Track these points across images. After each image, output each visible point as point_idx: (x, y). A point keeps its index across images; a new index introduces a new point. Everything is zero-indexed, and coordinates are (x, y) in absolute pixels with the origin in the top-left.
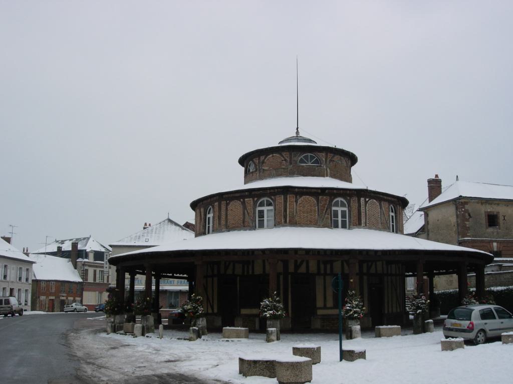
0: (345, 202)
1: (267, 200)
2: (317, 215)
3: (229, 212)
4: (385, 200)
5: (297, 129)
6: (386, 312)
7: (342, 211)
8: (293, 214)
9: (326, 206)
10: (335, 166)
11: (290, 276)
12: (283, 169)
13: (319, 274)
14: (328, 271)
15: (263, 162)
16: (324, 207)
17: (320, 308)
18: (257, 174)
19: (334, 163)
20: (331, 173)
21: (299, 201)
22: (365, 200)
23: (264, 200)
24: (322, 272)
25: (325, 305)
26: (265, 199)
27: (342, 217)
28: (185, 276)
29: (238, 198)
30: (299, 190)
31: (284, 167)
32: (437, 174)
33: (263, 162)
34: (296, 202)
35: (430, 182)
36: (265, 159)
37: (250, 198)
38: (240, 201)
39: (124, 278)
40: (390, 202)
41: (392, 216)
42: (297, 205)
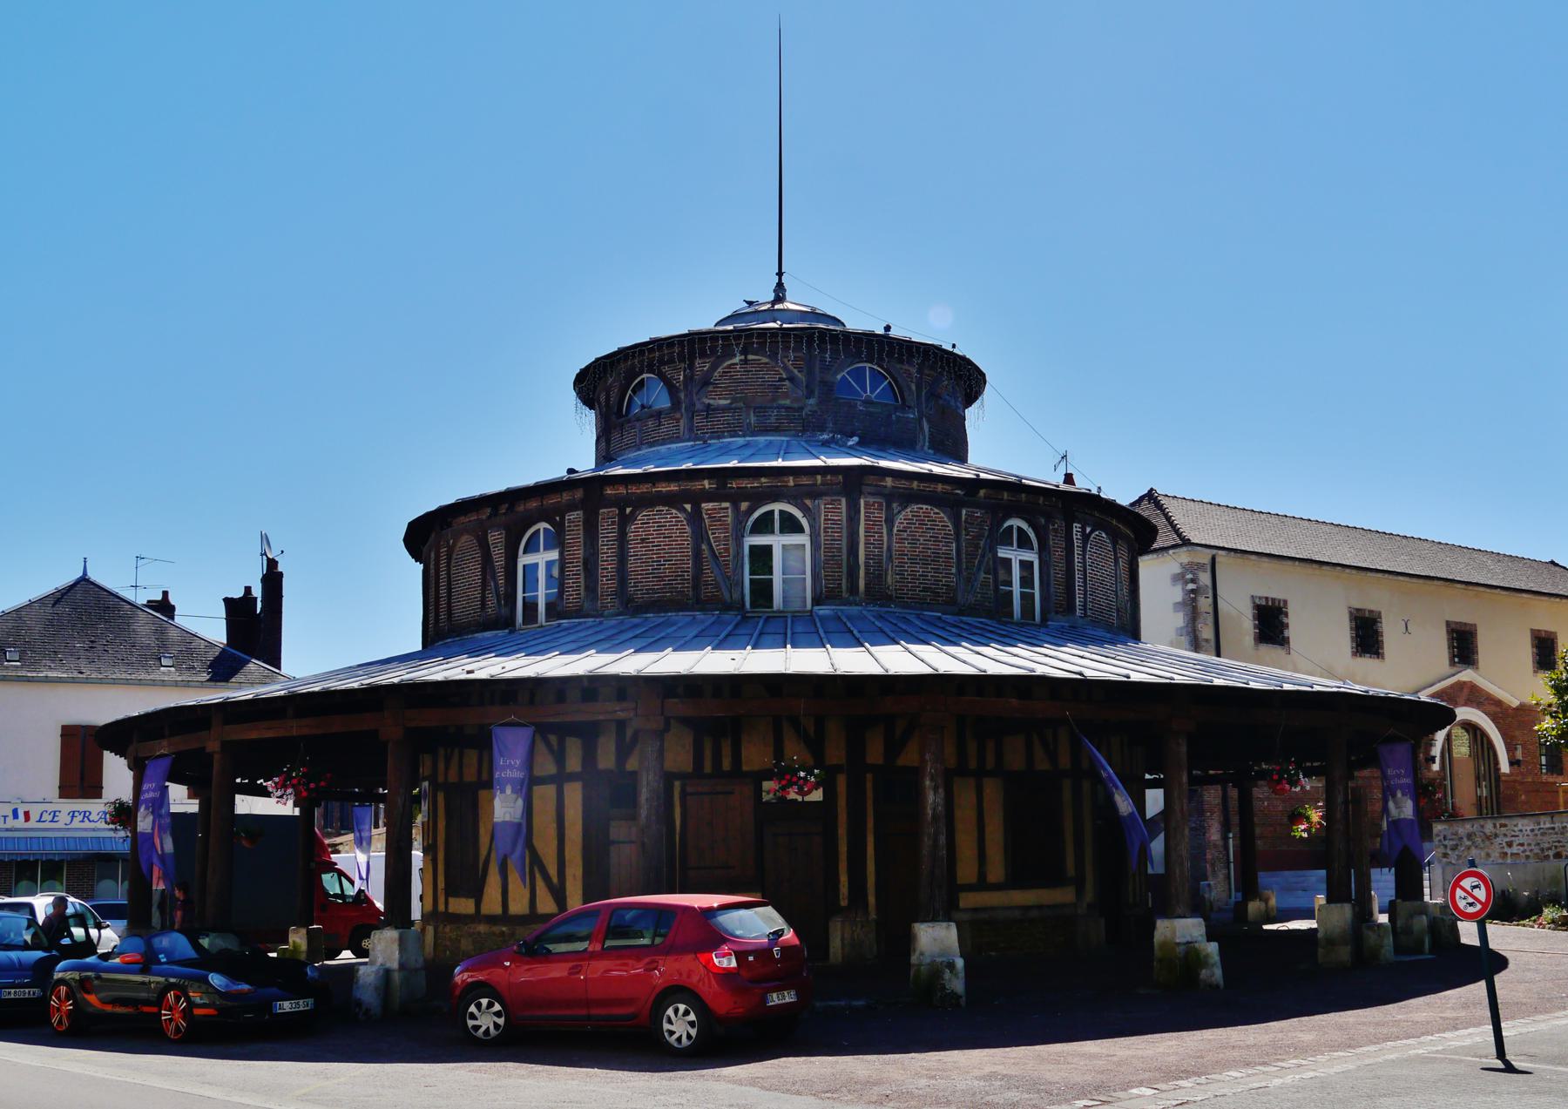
0: (1032, 535)
1: (781, 512)
2: (954, 570)
5: (780, 274)
8: (880, 562)
11: (869, 776)
12: (787, 408)
14: (990, 763)
15: (706, 382)
17: (970, 888)
18: (678, 420)
20: (931, 434)
21: (900, 521)
22: (1083, 529)
23: (772, 512)
24: (973, 764)
25: (982, 875)
27: (769, 584)
29: (672, 501)
31: (787, 402)
33: (706, 382)
34: (890, 522)
39: (672, 786)
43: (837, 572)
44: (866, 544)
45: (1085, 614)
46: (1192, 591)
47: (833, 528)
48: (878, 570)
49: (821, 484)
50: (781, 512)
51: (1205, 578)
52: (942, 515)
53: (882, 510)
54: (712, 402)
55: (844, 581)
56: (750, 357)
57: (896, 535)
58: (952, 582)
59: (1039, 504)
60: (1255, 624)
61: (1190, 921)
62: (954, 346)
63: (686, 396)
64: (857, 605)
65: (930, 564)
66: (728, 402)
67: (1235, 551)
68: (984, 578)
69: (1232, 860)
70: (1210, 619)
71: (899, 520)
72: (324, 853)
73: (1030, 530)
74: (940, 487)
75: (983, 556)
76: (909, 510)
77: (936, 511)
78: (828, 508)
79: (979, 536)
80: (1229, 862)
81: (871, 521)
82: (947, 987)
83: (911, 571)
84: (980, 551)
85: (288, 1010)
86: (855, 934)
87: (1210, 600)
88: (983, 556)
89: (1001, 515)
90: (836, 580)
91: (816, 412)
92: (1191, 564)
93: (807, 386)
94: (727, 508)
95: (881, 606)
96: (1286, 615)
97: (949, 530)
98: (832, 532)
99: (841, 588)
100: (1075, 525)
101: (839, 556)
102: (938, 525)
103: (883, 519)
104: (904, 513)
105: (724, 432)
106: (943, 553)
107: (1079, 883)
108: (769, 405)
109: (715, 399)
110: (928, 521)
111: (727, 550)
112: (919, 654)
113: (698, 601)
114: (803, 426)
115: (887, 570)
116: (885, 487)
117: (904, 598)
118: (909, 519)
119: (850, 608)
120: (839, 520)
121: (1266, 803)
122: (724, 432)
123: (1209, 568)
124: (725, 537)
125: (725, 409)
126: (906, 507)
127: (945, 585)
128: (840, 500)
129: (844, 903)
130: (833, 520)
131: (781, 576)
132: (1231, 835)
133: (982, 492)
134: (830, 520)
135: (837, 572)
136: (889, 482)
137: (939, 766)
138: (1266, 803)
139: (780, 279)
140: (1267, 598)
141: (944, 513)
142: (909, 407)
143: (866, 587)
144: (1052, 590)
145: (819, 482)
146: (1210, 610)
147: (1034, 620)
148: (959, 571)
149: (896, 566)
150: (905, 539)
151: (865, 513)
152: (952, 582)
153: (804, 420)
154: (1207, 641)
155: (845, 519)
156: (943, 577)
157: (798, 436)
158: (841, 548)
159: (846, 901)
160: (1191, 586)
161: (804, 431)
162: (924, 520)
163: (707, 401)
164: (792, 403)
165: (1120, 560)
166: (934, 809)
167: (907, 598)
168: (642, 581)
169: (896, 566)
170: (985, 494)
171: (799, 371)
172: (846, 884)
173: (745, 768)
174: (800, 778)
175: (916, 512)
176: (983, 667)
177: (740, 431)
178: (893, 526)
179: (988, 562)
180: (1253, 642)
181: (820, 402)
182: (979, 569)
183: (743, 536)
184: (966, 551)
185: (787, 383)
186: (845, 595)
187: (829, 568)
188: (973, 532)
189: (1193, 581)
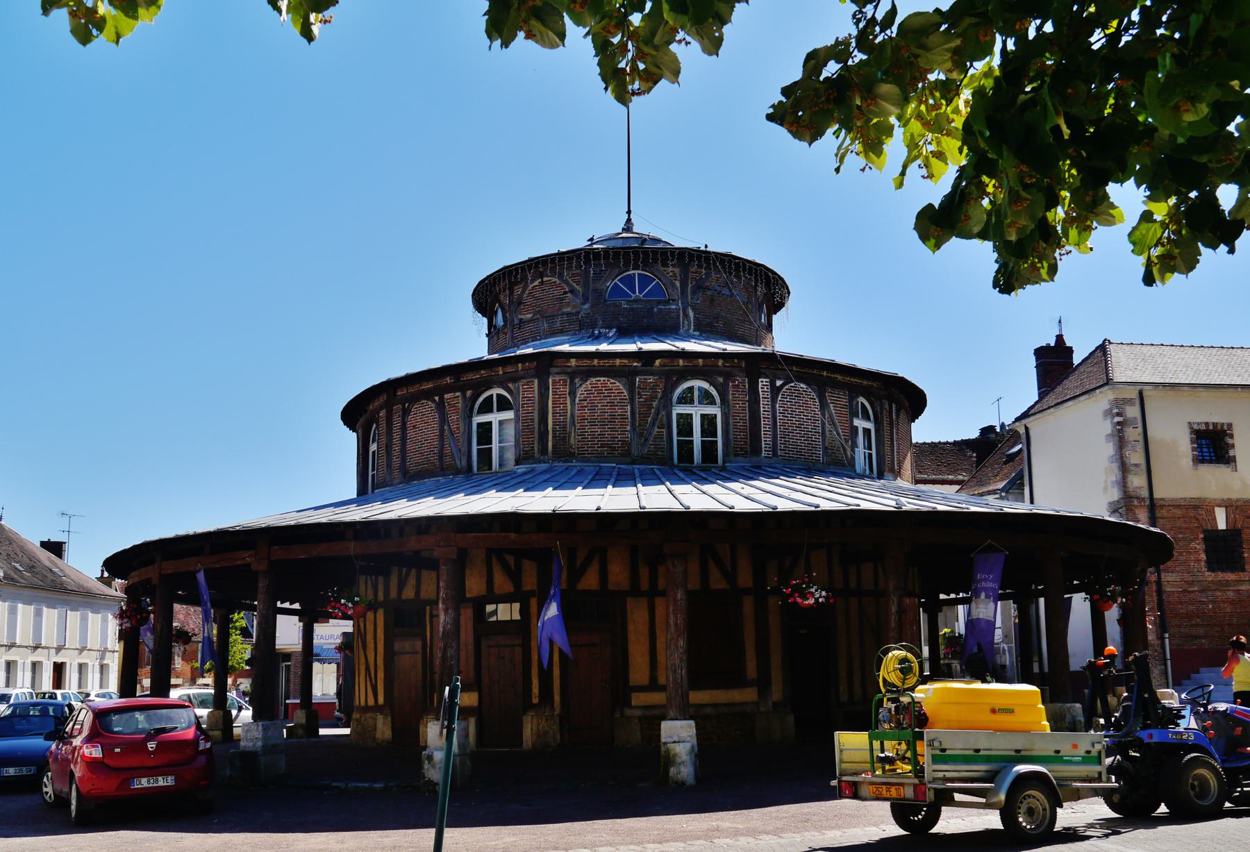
1: (497, 395)
2: (628, 428)
3: (410, 434)
4: (837, 385)
5: (629, 212)
6: (844, 698)
7: (703, 416)
8: (565, 427)
9: (655, 404)
10: (712, 300)
12: (568, 314)
13: (635, 591)
16: (650, 407)
19: (709, 293)
20: (696, 319)
21: (580, 393)
22: (772, 384)
23: (492, 395)
24: (645, 586)
26: (495, 391)
27: (704, 433)
28: (297, 606)
29: (428, 395)
30: (581, 363)
31: (569, 309)
32: (43, 16)
34: (573, 394)
35: (1041, 353)
36: (523, 292)
37: (454, 391)
38: (434, 401)
40: (854, 391)
41: (867, 432)
42: (573, 401)
43: (530, 438)
44: (553, 413)
45: (775, 454)
46: (1119, 423)
47: (528, 404)
48: (562, 434)
49: (522, 370)
50: (497, 395)
51: (1133, 412)
52: (618, 384)
53: (566, 385)
54: (523, 317)
55: (536, 445)
56: (545, 279)
57: (578, 404)
58: (628, 438)
59: (718, 366)
60: (1193, 448)
61: (678, 723)
62: (706, 246)
63: (510, 315)
64: (544, 463)
65: (607, 425)
66: (532, 315)
67: (1164, 385)
68: (657, 432)
69: (1169, 658)
70: (1140, 446)
71: (580, 392)
72: (1156, 623)
73: (712, 388)
74: (618, 362)
75: (657, 414)
76: (588, 383)
77: (613, 381)
78: (525, 388)
79: (652, 398)
80: (1165, 659)
81: (558, 395)
82: (426, 776)
83: (591, 432)
84: (653, 411)
85: (12, 774)
86: (541, 726)
87: (1140, 429)
88: (657, 414)
89: (675, 379)
90: (531, 444)
91: (589, 314)
92: (1116, 400)
93: (583, 295)
94: (458, 397)
95: (564, 462)
96: (1232, 436)
97: (624, 396)
98: (527, 407)
99: (534, 450)
100: (760, 380)
101: (532, 425)
102: (614, 393)
103: (567, 393)
104: (584, 386)
105: (528, 338)
106: (619, 415)
107: (763, 684)
108: (556, 314)
109: (525, 314)
110: (605, 390)
111: (458, 428)
112: (710, 492)
113: (442, 469)
114: (580, 326)
115: (570, 433)
116: (570, 366)
117: (585, 454)
118: (589, 390)
119: (540, 465)
120: (532, 397)
121: (1211, 606)
122: (528, 338)
123: (1138, 402)
124: (457, 418)
125: (530, 321)
126: (586, 381)
127: (620, 441)
128: (533, 381)
129: (535, 701)
130: (528, 397)
131: (700, 439)
132: (1167, 635)
133: (658, 362)
134: (526, 397)
135: (530, 438)
136: (573, 362)
137: (449, 591)
138: (1211, 606)
139: (629, 216)
140: (1207, 424)
141: (619, 382)
142: (674, 300)
143: (553, 448)
144: (731, 436)
145: (520, 369)
146: (1141, 438)
147: (717, 463)
148: (633, 425)
149: (578, 429)
150: (586, 407)
151: (553, 389)
152: (628, 438)
153: (580, 321)
154: (1136, 465)
155: (537, 397)
156: (618, 434)
157: (576, 334)
158: (533, 419)
159: (537, 700)
160: (1117, 419)
161: (580, 330)
162: (602, 390)
163: (520, 317)
164: (572, 309)
165: (831, 405)
166: (444, 627)
167: (588, 454)
168: (413, 460)
169: (578, 429)
170: (660, 363)
171: (577, 285)
172: (537, 686)
173: (468, 595)
174: (342, 605)
175: (595, 384)
176: (730, 504)
177: (538, 336)
178: (575, 397)
179: (661, 418)
180: (1191, 463)
181: (592, 307)
182: (654, 425)
183: (472, 417)
184: (640, 411)
185: (569, 295)
186: (537, 455)
187: (525, 435)
188: (644, 395)
189: (1118, 414)
